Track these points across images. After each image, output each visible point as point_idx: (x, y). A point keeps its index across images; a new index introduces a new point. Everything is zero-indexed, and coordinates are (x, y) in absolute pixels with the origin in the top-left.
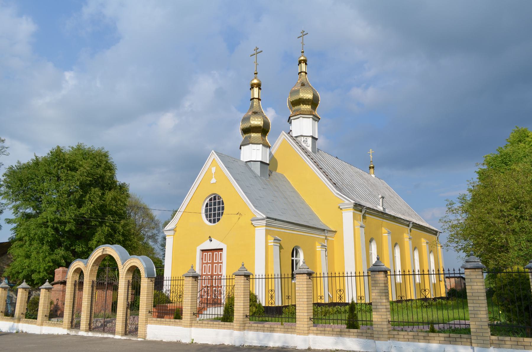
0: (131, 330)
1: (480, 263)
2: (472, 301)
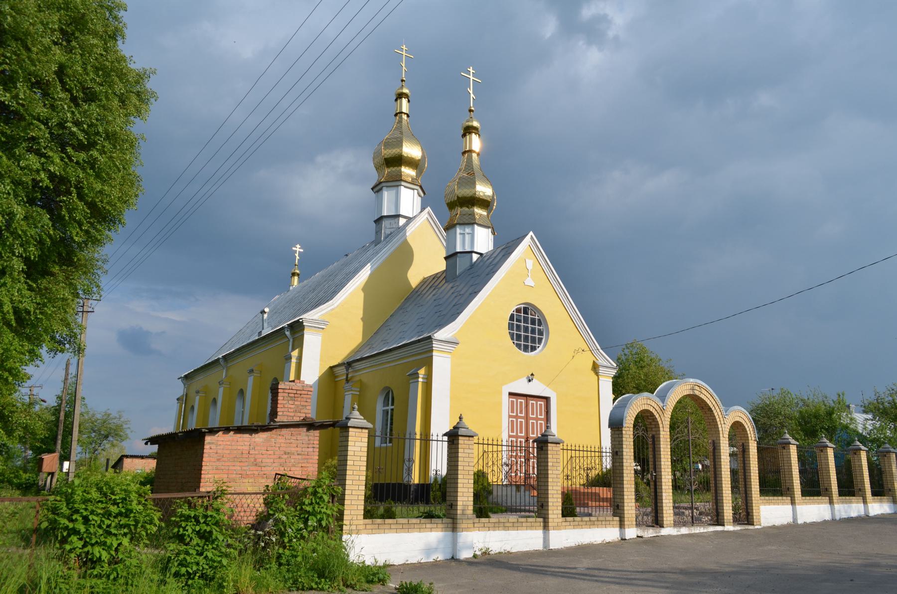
0: (744, 515)
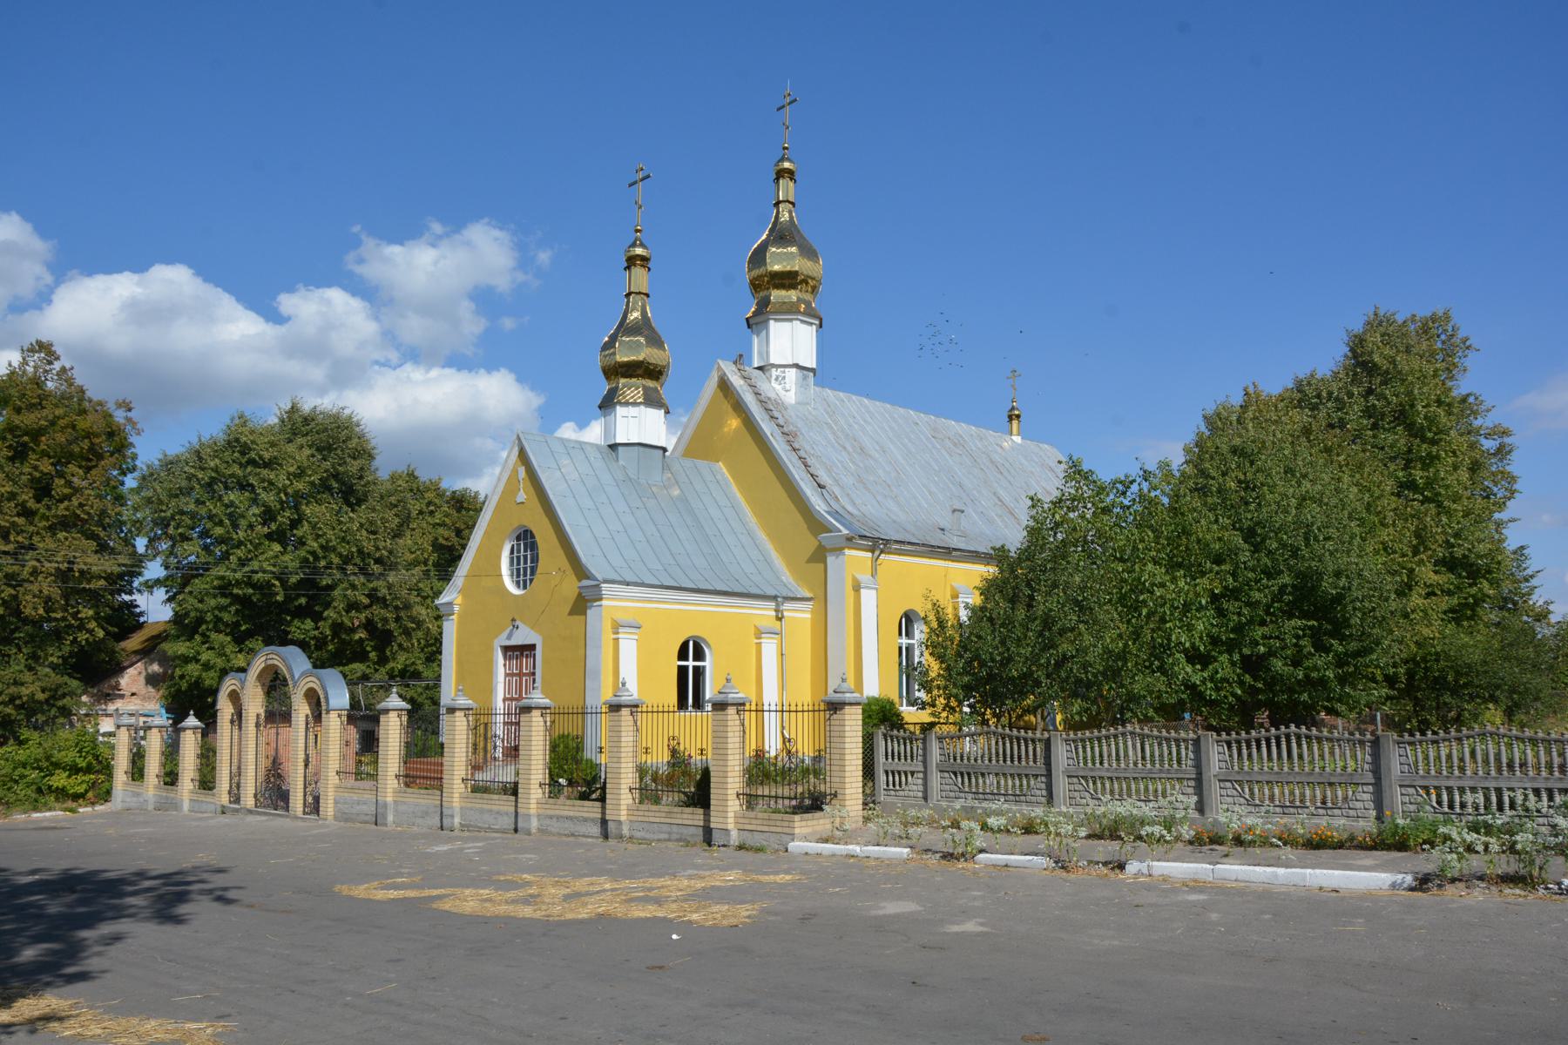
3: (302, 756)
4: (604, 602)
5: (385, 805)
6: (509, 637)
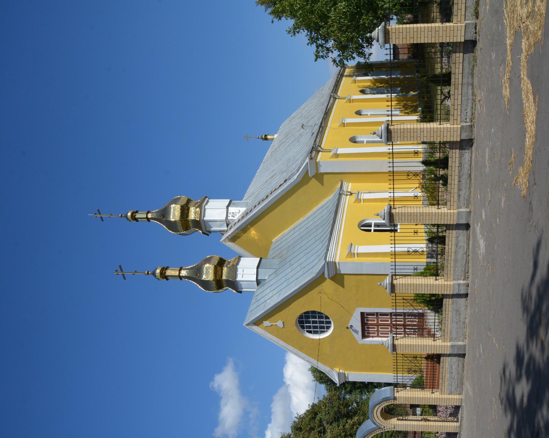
1: (380, 27)
2: (419, 39)
3: (423, 423)
4: (337, 261)
5: (452, 347)
6: (357, 332)
